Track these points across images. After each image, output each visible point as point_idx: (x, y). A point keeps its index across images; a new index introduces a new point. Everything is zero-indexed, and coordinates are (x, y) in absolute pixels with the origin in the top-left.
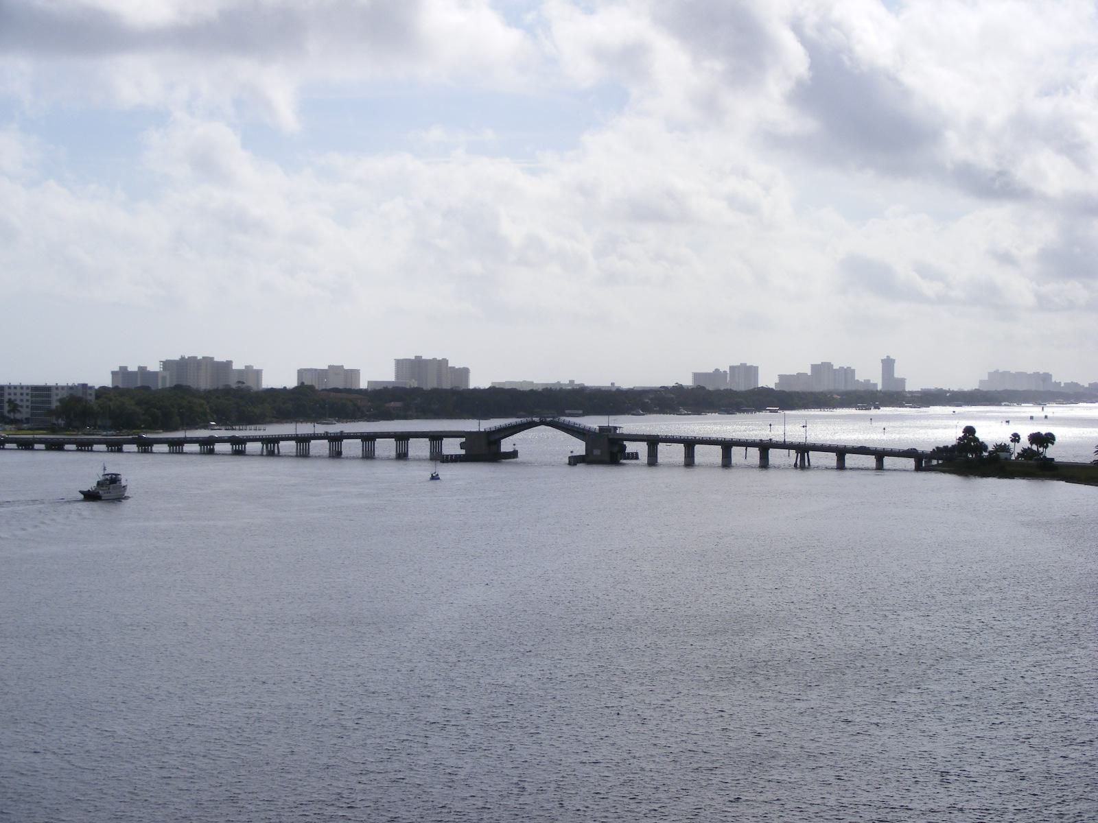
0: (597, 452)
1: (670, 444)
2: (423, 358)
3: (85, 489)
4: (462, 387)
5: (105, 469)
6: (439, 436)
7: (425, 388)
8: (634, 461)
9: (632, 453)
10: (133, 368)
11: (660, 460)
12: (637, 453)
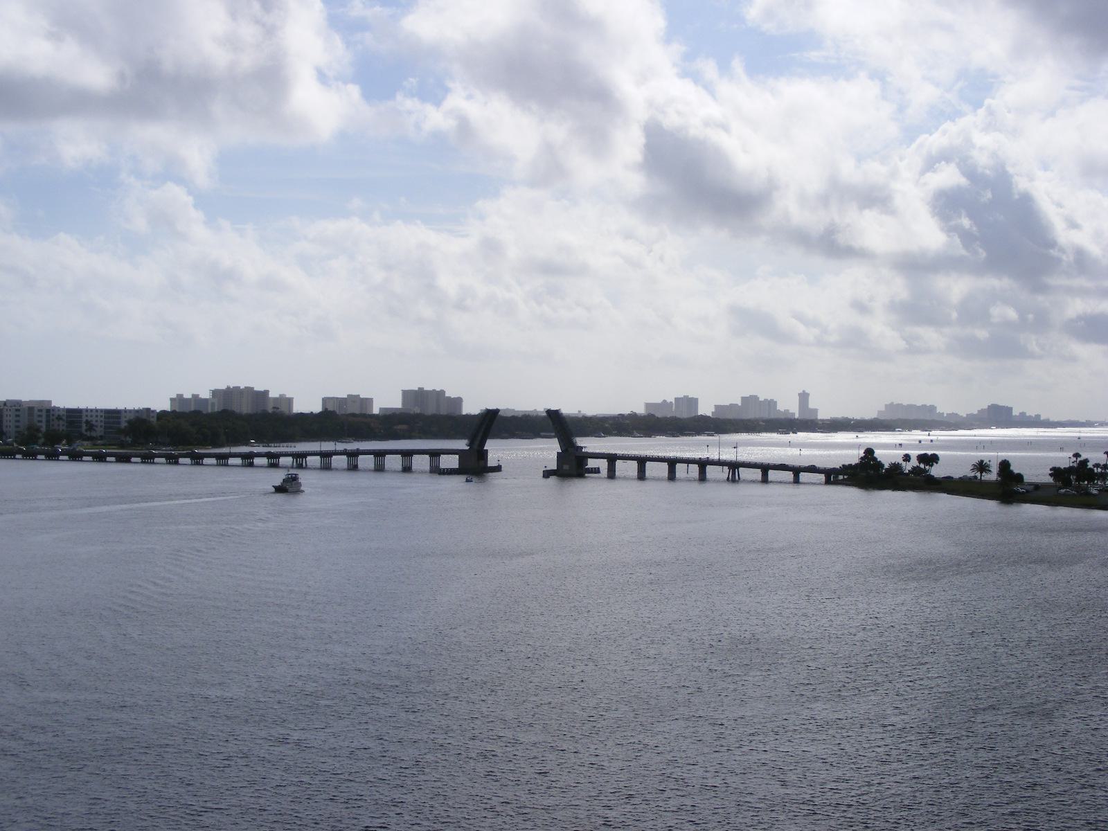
0: (566, 467)
4: (457, 413)
7: (426, 414)
9: (595, 468)
10: (188, 395)
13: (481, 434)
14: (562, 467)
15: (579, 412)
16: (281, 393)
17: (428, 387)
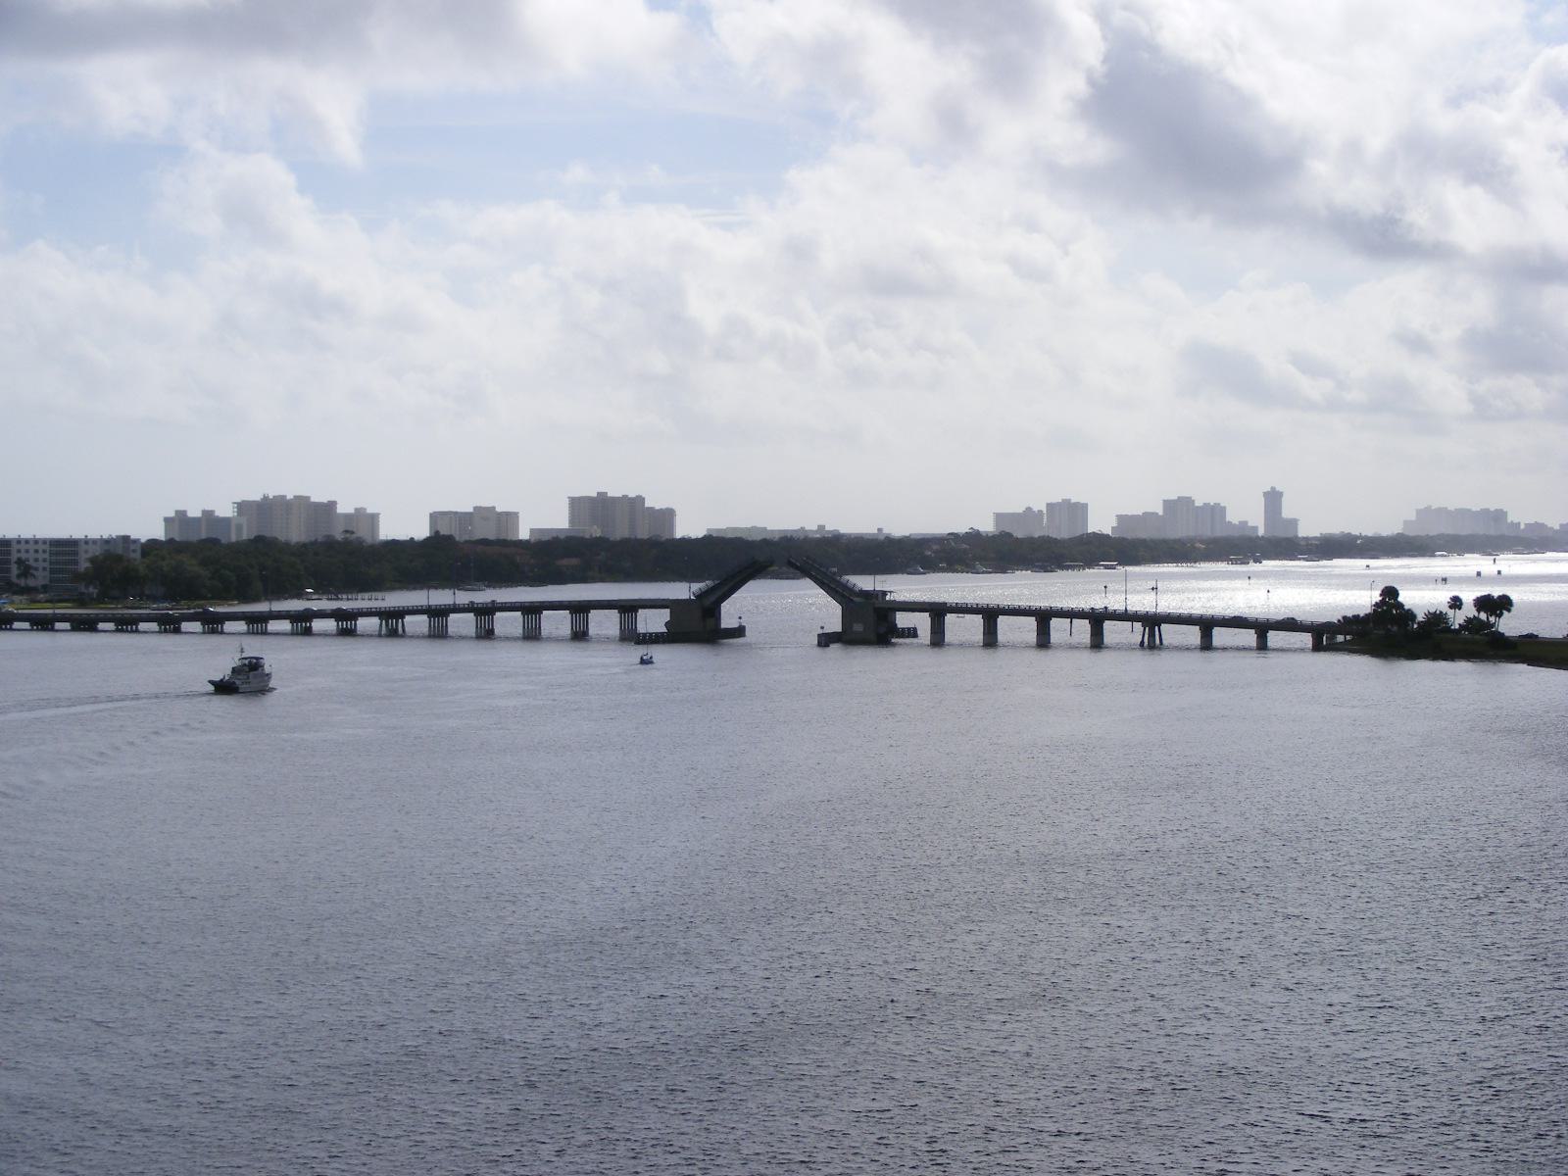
0: (858, 627)
2: (609, 495)
3: (217, 678)
4: (666, 536)
9: (909, 629)
10: (194, 512)
11: (948, 637)
16: (358, 507)
17: (614, 492)
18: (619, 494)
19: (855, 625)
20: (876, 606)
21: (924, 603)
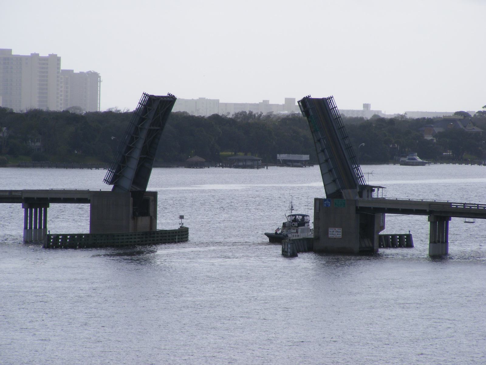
1: (471, 220)
2: (14, 53)
3: (272, 231)
4: (86, 108)
5: (292, 209)
6: (39, 199)
7: (16, 110)
8: (405, 251)
9: (401, 236)
11: (453, 248)
12: (409, 237)
13: (137, 154)
14: (327, 233)
15: (366, 106)
18: (26, 52)
19: (331, 230)
20: (360, 205)
21: (421, 203)
